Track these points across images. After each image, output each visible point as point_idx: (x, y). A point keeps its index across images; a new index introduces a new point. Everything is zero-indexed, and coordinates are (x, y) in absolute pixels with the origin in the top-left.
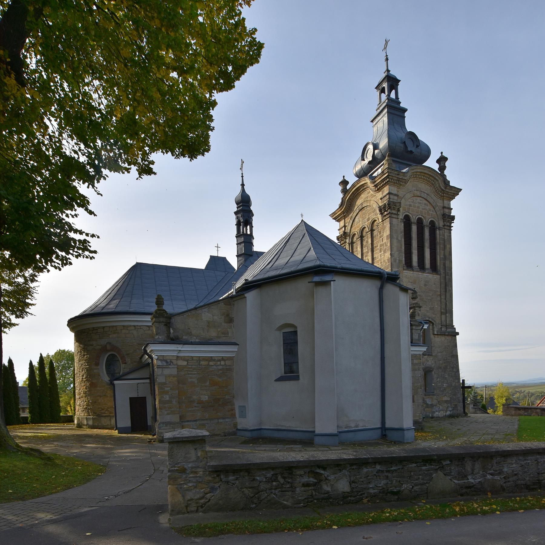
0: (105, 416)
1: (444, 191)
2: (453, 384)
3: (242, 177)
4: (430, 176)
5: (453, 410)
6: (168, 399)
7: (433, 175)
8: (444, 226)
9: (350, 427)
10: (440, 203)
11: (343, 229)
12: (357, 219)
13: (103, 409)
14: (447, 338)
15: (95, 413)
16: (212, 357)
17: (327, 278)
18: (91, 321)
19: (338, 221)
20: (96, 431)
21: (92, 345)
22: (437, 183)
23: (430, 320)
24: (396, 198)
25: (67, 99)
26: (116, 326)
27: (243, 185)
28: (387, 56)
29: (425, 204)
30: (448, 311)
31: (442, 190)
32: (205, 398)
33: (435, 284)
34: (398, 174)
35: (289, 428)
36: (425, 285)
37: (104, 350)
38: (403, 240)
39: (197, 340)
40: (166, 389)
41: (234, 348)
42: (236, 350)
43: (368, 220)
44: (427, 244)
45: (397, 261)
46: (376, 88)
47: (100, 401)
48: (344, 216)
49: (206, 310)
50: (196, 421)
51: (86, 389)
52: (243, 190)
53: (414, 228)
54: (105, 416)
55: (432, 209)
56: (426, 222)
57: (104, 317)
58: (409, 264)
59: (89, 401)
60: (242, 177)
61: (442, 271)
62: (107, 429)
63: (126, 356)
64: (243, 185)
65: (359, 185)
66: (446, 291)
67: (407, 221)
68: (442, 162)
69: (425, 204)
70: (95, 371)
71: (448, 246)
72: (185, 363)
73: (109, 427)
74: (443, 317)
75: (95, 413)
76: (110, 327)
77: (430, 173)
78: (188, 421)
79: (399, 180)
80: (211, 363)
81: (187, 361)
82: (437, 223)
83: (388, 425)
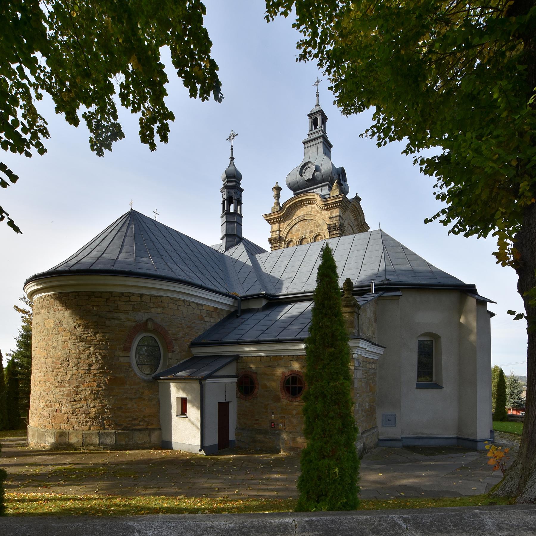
0: (140, 430)
3: (232, 149)
11: (278, 233)
12: (295, 228)
13: (135, 419)
15: (120, 425)
18: (115, 282)
19: (271, 223)
20: (130, 454)
21: (118, 319)
25: (485, 61)
26: (161, 297)
27: (232, 159)
35: (430, 436)
37: (142, 327)
41: (380, 351)
42: (382, 353)
43: (311, 232)
46: (308, 115)
47: (129, 406)
48: (280, 221)
51: (99, 386)
54: (140, 430)
57: (130, 279)
59: (103, 406)
60: (232, 149)
62: (144, 449)
63: (174, 341)
64: (232, 159)
65: (305, 198)
70: (122, 359)
73: (148, 445)
75: (120, 425)
76: (151, 296)
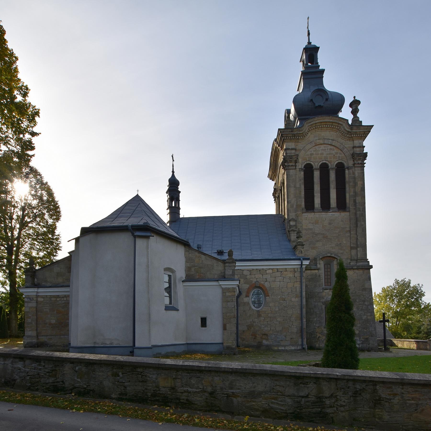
1: (350, 132)
2: (364, 317)
3: (173, 166)
4: (333, 122)
5: (362, 343)
6: (30, 321)
7: (336, 121)
8: (354, 164)
9: (105, 344)
10: (349, 144)
14: (357, 271)
16: (58, 295)
17: (148, 234)
19: (273, 180)
22: (342, 127)
23: (333, 256)
24: (294, 151)
27: (173, 172)
28: (309, 31)
29: (331, 149)
30: (361, 245)
31: (349, 132)
32: (53, 321)
33: (342, 221)
34: (292, 131)
36: (330, 224)
38: (303, 187)
39: (50, 285)
40: (30, 315)
44: (317, 188)
45: (295, 206)
49: (56, 265)
50: (47, 336)
52: (173, 175)
53: (317, 174)
55: (340, 151)
56: (332, 164)
58: (309, 206)
60: (173, 166)
61: (352, 208)
64: (173, 172)
66: (357, 226)
67: (308, 170)
68: (353, 106)
69: (331, 149)
71: (359, 183)
72: (42, 299)
74: (354, 252)
77: (331, 121)
78: (42, 336)
79: (294, 135)
80: (58, 299)
81: (43, 298)
82: (345, 164)
83: (137, 345)
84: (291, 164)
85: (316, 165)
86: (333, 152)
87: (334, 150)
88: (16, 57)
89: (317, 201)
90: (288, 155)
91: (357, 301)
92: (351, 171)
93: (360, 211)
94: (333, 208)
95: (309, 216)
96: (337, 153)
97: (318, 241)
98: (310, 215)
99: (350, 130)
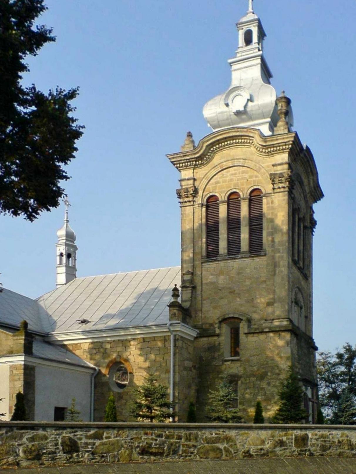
8: (274, 189)
22: (254, 140)
29: (243, 172)
36: (239, 274)
44: (296, 241)
67: (211, 203)
69: (243, 172)
84: (186, 199)
85: (222, 196)
86: (247, 176)
87: (247, 173)
88: (35, 211)
89: (223, 245)
90: (184, 187)
91: (269, 374)
92: (269, 199)
93: (279, 252)
94: (244, 252)
95: (210, 266)
96: (251, 177)
97: (222, 298)
98: (211, 266)
99: (264, 144)
